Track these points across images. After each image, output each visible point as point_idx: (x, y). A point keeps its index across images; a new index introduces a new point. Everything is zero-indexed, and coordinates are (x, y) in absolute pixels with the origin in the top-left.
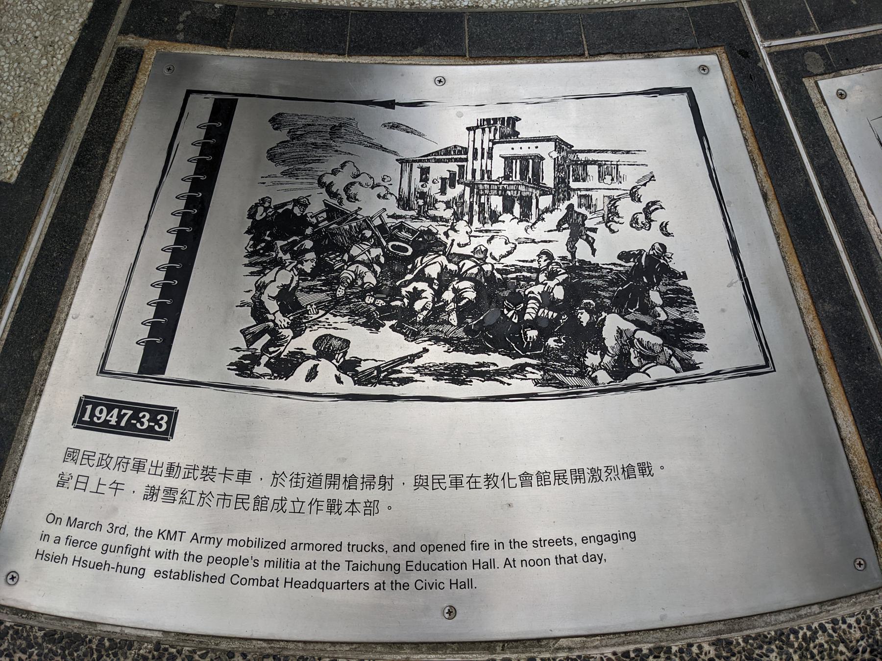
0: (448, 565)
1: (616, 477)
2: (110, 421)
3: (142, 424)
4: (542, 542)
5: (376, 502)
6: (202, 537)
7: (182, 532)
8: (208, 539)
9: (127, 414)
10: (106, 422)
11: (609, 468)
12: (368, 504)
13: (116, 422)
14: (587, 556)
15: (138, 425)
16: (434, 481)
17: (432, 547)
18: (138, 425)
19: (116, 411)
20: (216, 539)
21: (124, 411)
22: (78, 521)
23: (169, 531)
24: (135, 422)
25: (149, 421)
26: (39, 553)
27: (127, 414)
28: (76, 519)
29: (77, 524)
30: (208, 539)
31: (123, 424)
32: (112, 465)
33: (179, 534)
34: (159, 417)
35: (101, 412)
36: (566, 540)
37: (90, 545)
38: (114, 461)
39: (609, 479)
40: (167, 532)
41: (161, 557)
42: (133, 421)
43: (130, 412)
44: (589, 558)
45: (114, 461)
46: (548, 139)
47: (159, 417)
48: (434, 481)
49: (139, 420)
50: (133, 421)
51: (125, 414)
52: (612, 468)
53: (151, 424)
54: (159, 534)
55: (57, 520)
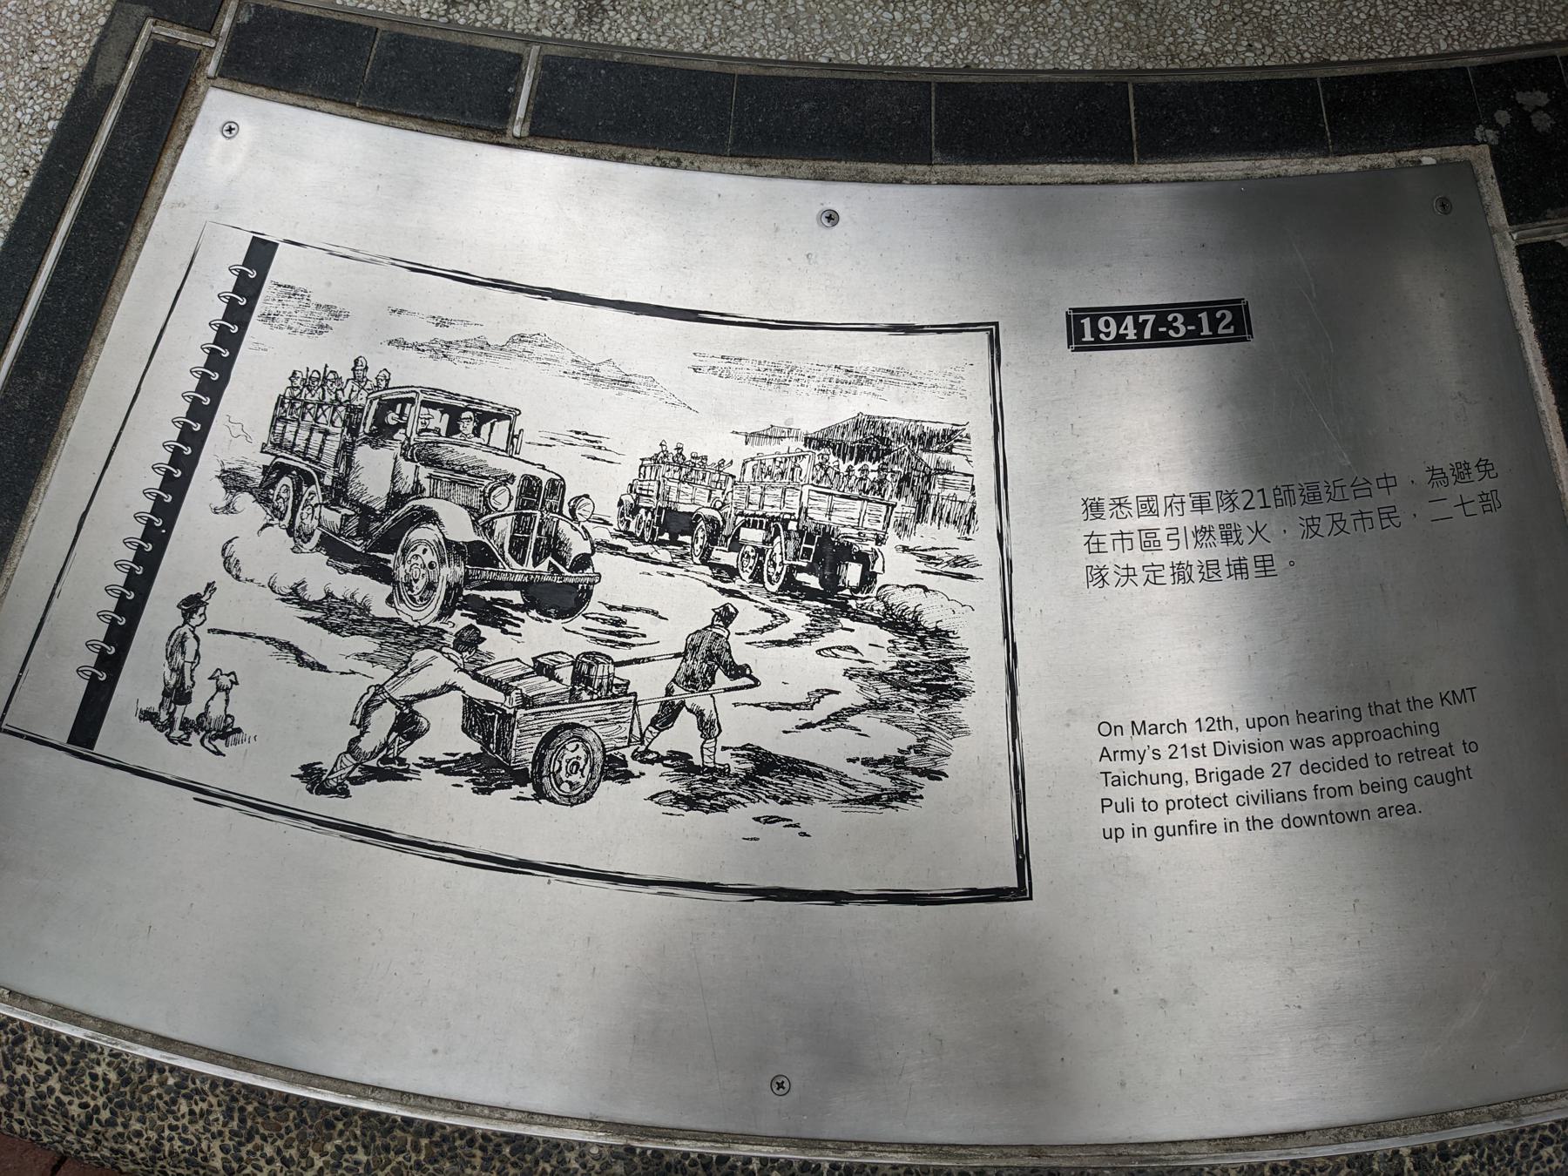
2: (1127, 335)
3: (1177, 330)
4: (1420, 754)
5: (1494, 493)
6: (1115, 752)
7: (1471, 689)
8: (1125, 754)
9: (1148, 320)
10: (1120, 338)
12: (1484, 497)
13: (1135, 334)
15: (1171, 333)
16: (1382, 516)
18: (1171, 333)
19: (1129, 320)
20: (1136, 753)
21: (1142, 318)
23: (1453, 692)
24: (1164, 329)
27: (1148, 320)
28: (1144, 722)
30: (1125, 754)
31: (1147, 335)
33: (1468, 693)
34: (1170, 318)
35: (1107, 324)
40: (1450, 693)
43: (1152, 318)
47: (1170, 318)
48: (1382, 516)
49: (1170, 326)
50: (1161, 329)
51: (1146, 321)
53: (1189, 328)
54: (1442, 700)
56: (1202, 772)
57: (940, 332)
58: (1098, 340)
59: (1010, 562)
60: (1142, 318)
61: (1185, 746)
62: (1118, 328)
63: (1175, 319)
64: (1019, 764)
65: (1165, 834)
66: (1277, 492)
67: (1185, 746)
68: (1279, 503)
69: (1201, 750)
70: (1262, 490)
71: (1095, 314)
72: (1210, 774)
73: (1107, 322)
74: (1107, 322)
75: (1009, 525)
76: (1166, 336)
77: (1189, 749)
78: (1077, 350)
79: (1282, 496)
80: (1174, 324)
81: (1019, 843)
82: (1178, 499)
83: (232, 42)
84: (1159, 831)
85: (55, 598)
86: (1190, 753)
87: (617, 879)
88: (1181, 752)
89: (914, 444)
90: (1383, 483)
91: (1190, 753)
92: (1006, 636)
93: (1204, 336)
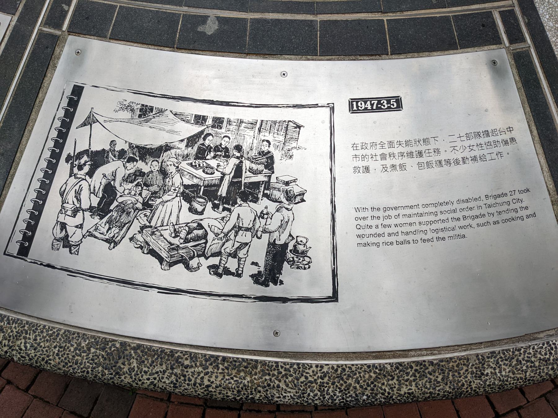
3: (384, 106)
15: (382, 107)
18: (382, 107)
19: (369, 102)
25: (387, 104)
26: (521, 411)
31: (374, 108)
32: (368, 147)
37: (516, 201)
38: (369, 145)
42: (379, 106)
45: (369, 145)
46: (305, 237)
47: (382, 102)
49: (382, 104)
50: (379, 106)
51: (374, 103)
57: (310, 107)
59: (335, 178)
60: (372, 102)
63: (384, 102)
64: (335, 244)
71: (357, 100)
73: (361, 103)
74: (361, 103)
75: (335, 166)
76: (380, 108)
81: (333, 271)
82: (375, 144)
85: (23, 207)
87: (209, 294)
89: (68, 361)
90: (509, 130)
92: (332, 202)
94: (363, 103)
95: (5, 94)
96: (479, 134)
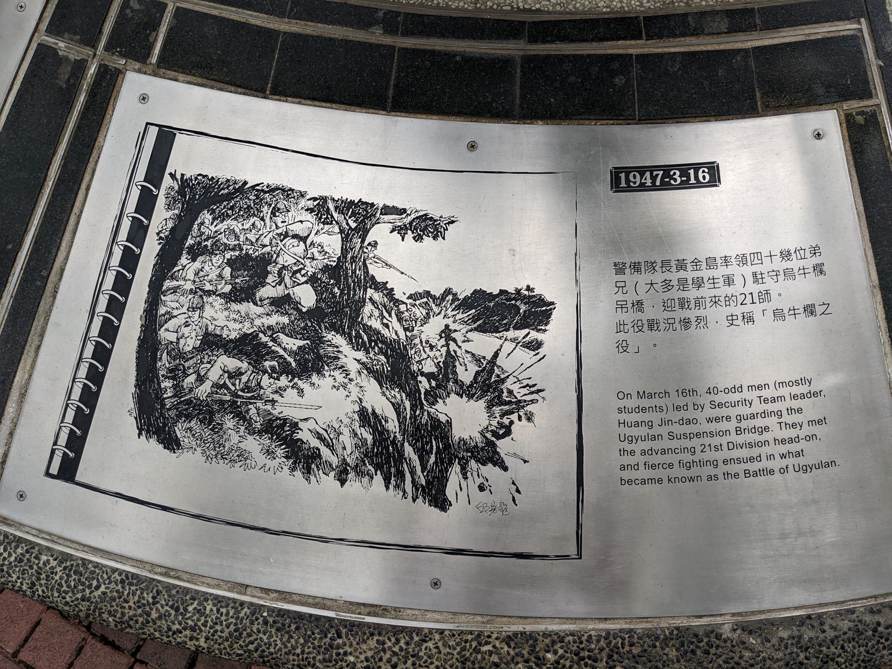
0: (702, 463)
1: (705, 326)
2: (646, 183)
3: (675, 180)
9: (658, 174)
10: (642, 185)
11: (699, 318)
13: (651, 183)
14: (683, 420)
15: (672, 182)
17: (733, 391)
18: (672, 182)
19: (648, 174)
21: (655, 173)
22: (646, 393)
24: (668, 180)
25: (680, 176)
27: (658, 174)
28: (644, 392)
29: (646, 395)
31: (658, 183)
34: (672, 173)
35: (635, 177)
36: (657, 408)
39: (699, 327)
41: (785, 458)
42: (666, 180)
44: (685, 422)
47: (672, 173)
49: (671, 177)
50: (666, 180)
52: (702, 318)
53: (683, 179)
55: (628, 396)
56: (739, 429)
58: (629, 186)
60: (655, 173)
61: (710, 445)
62: (641, 180)
65: (742, 419)
66: (760, 294)
67: (710, 445)
68: (761, 301)
69: (719, 447)
70: (752, 293)
71: (628, 170)
72: (744, 429)
73: (634, 175)
74: (634, 175)
76: (669, 184)
77: (712, 446)
78: (616, 191)
79: (763, 297)
80: (674, 177)
83: (740, 114)
84: (739, 418)
86: (713, 449)
88: (707, 448)
91: (713, 449)
93: (691, 184)
94: (637, 175)
95: (52, 151)
96: (654, 265)
